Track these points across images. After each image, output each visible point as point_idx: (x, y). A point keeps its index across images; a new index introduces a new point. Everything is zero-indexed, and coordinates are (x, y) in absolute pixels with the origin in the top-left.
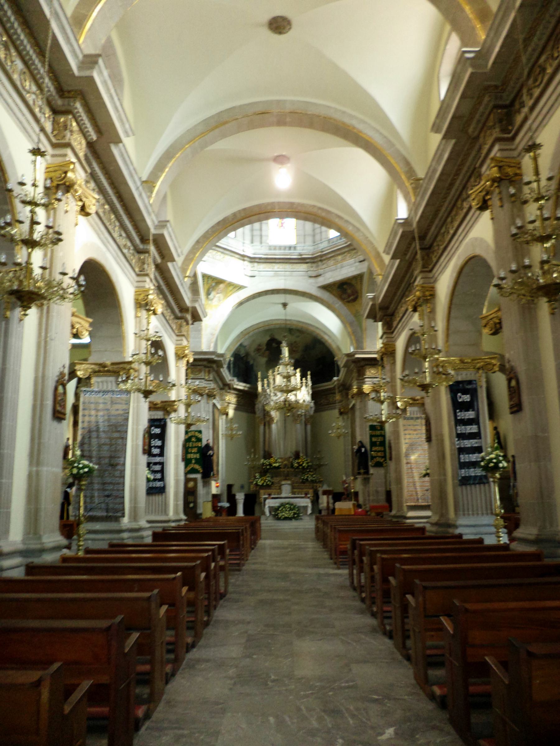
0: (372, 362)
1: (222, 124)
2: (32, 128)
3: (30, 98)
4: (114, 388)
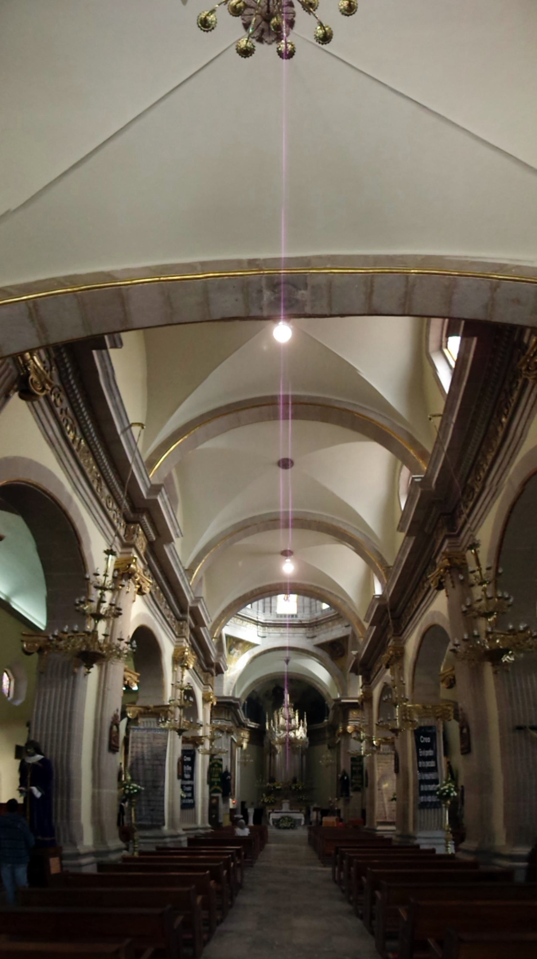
0: (354, 706)
1: (245, 528)
2: (110, 533)
3: (111, 513)
4: (156, 727)
